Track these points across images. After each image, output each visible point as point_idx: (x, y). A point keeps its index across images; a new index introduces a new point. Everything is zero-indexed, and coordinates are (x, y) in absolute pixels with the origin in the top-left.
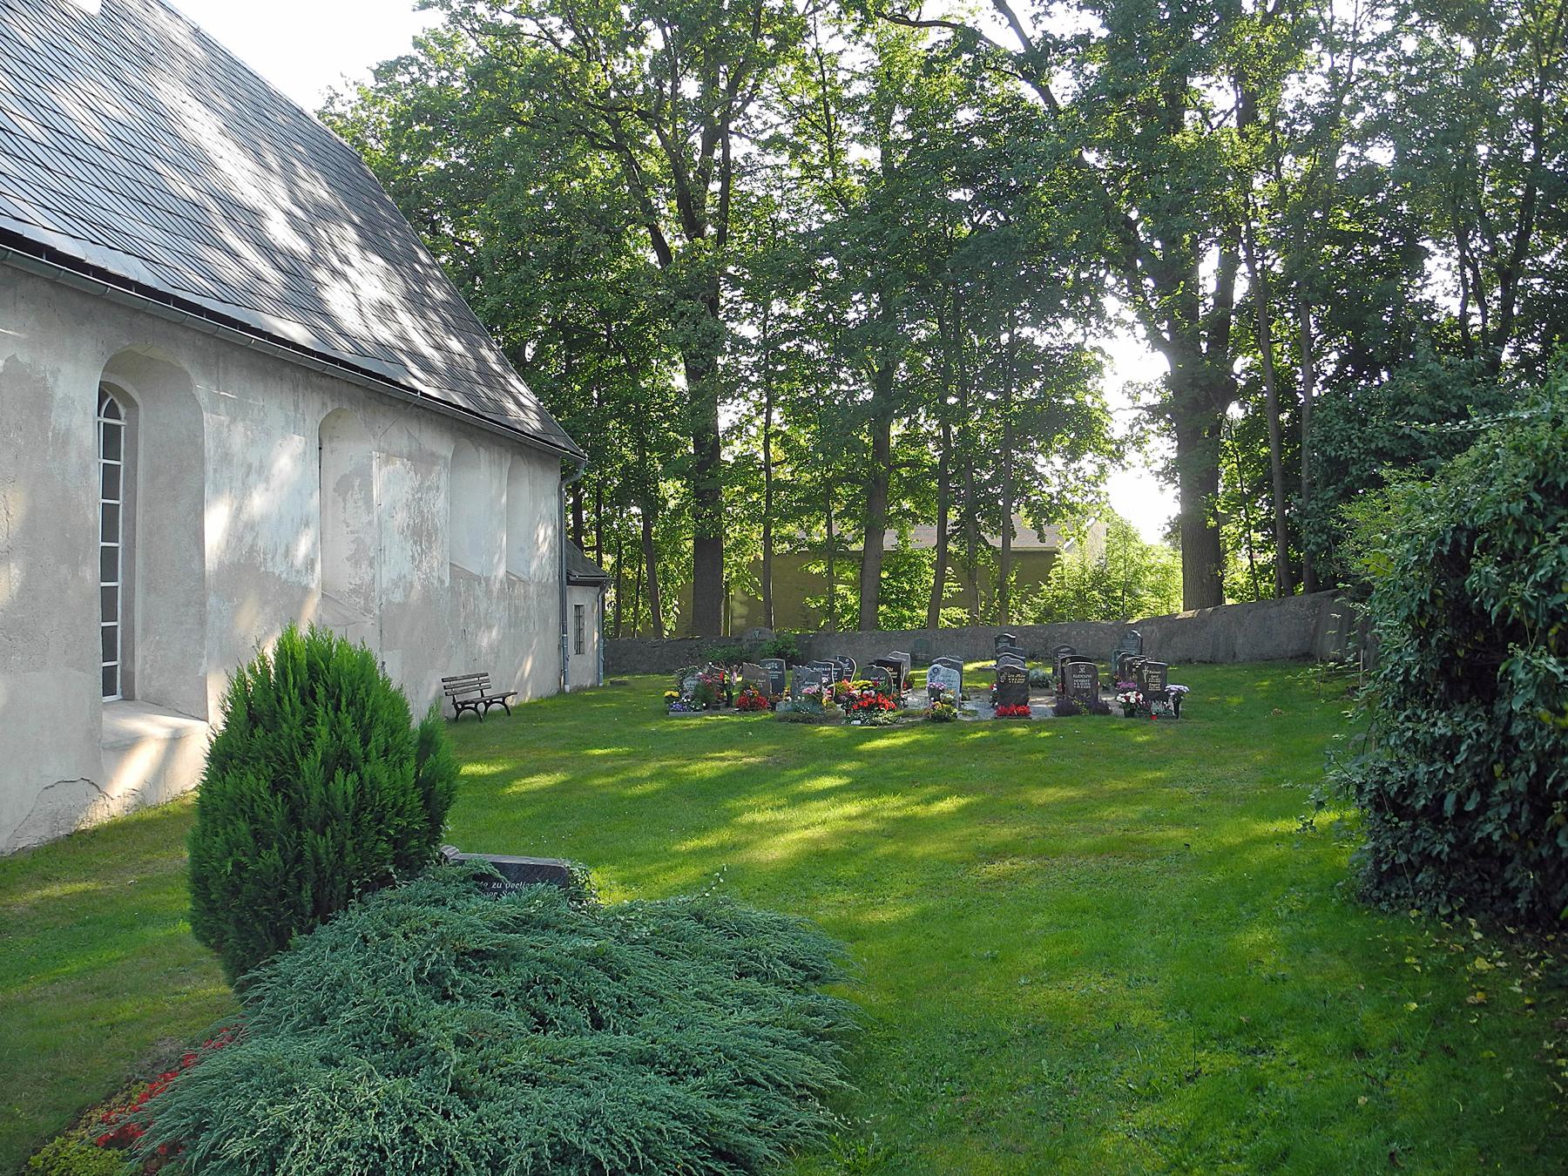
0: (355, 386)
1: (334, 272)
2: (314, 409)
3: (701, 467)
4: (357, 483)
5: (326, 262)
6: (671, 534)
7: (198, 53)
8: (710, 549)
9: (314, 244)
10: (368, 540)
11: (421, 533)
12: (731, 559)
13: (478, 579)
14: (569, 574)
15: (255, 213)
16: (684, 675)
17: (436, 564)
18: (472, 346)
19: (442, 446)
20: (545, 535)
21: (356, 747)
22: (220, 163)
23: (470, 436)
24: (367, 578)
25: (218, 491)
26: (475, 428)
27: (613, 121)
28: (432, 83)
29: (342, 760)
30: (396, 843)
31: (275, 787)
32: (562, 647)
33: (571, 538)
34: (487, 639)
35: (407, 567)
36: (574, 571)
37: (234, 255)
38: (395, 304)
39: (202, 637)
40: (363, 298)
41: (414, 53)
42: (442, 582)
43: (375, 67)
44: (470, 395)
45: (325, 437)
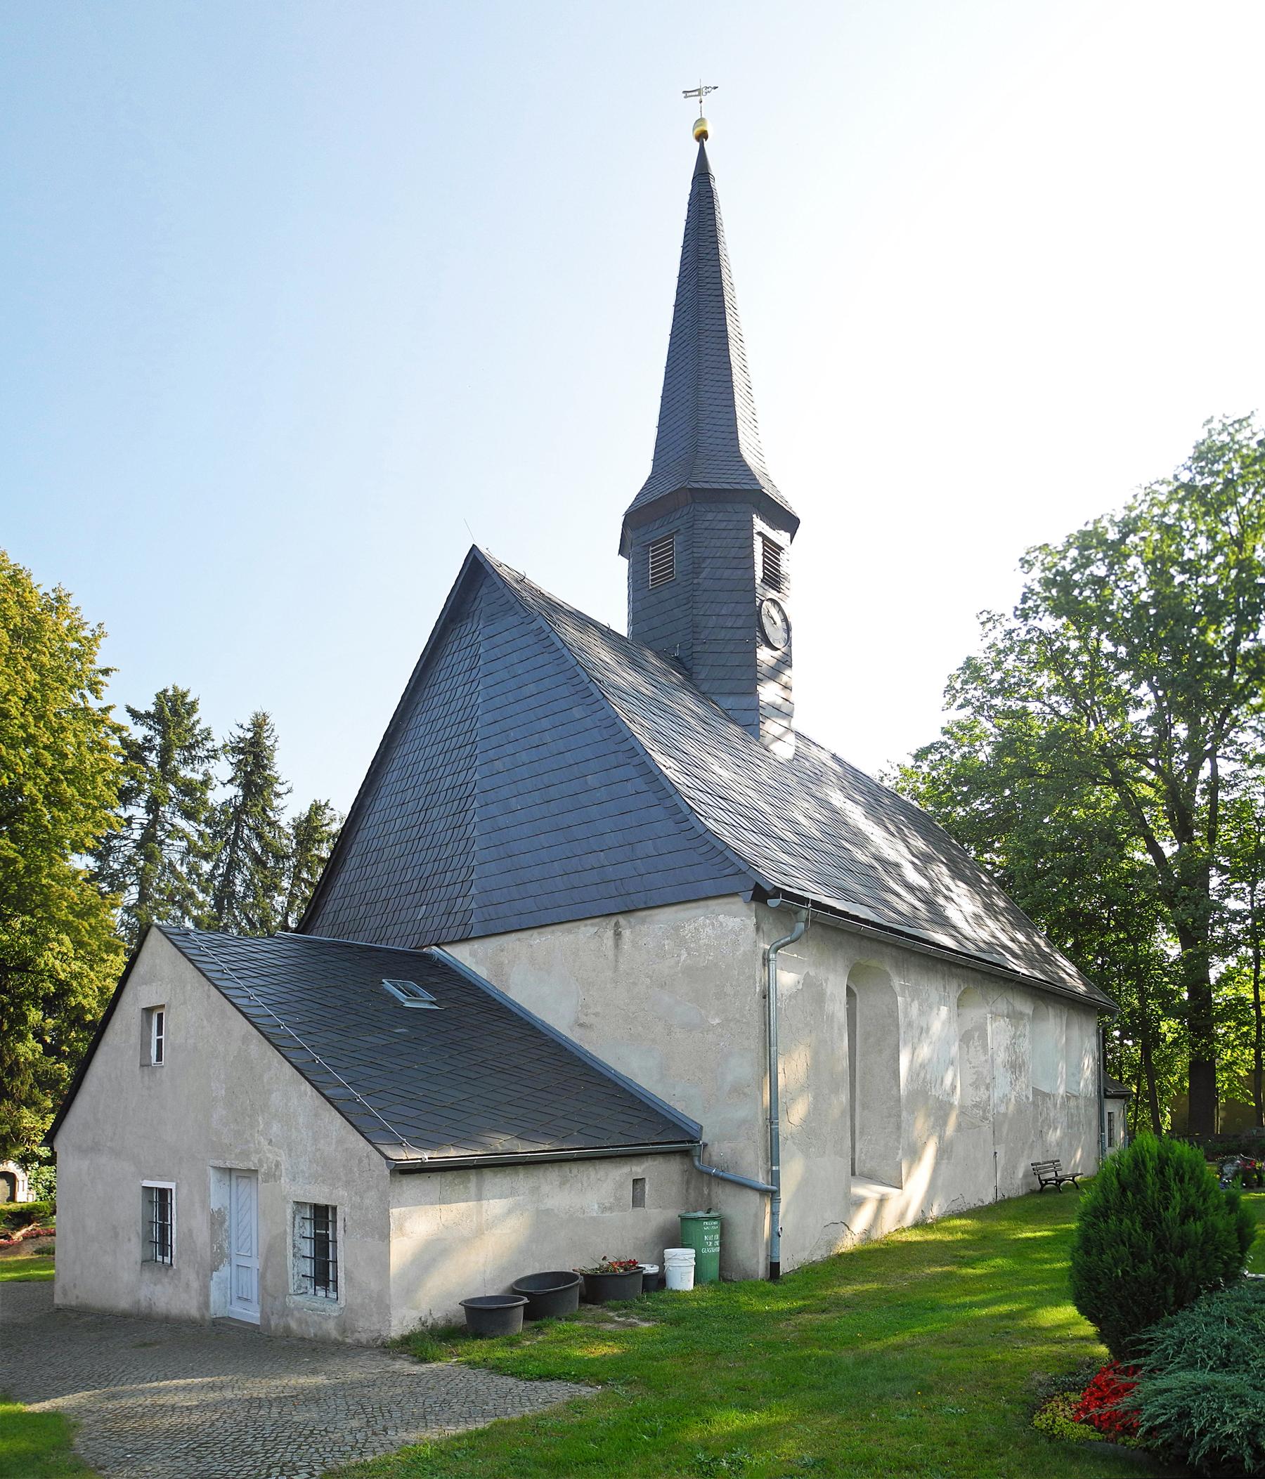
0: (976, 972)
1: (946, 897)
2: (954, 990)
3: (1197, 1009)
4: (976, 1035)
5: (940, 892)
6: (1167, 1060)
7: (838, 769)
8: (1202, 1070)
9: (931, 881)
10: (985, 1073)
11: (1016, 1066)
12: (1222, 1076)
13: (1048, 1095)
14: (1105, 1090)
15: (897, 865)
16: (1224, 1163)
17: (1023, 1088)
18: (1028, 937)
19: (1024, 1006)
20: (1088, 1064)
21: (1200, 1205)
22: (872, 837)
23: (1042, 999)
24: (985, 1097)
25: (905, 1044)
26: (1047, 994)
27: (1110, 764)
28: (956, 757)
29: (1189, 1213)
30: (1226, 1264)
31: (1146, 1226)
32: (1100, 1141)
33: (1106, 1066)
34: (1054, 1136)
35: (1007, 1089)
36: (1108, 1089)
37: (898, 895)
38: (983, 914)
39: (899, 1137)
40: (968, 916)
41: (944, 739)
42: (1027, 1098)
43: (914, 752)
44: (1043, 972)
45: (960, 1003)
